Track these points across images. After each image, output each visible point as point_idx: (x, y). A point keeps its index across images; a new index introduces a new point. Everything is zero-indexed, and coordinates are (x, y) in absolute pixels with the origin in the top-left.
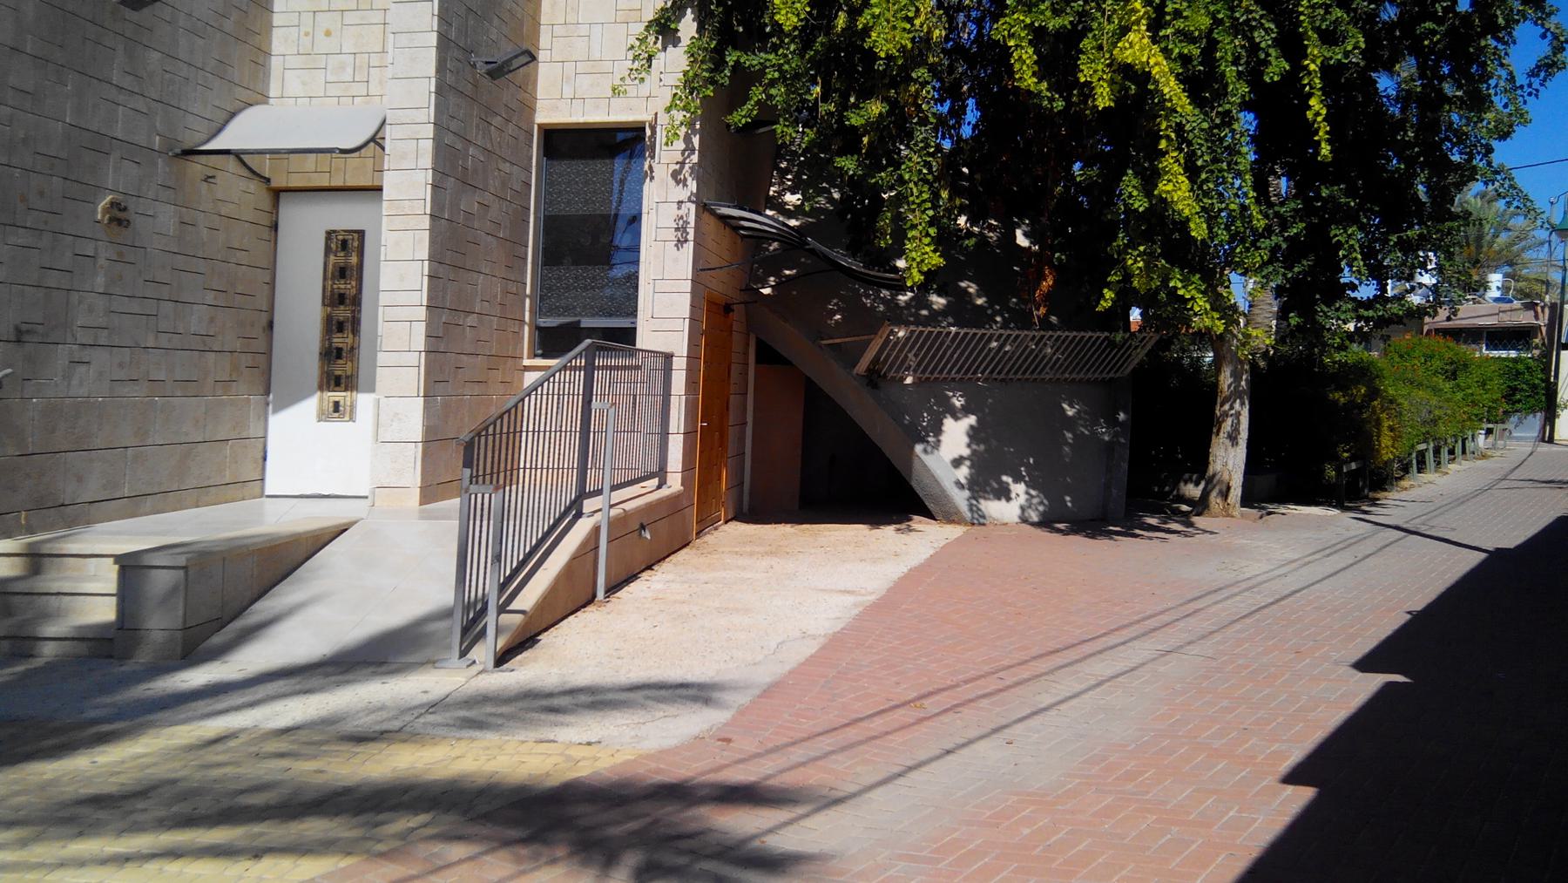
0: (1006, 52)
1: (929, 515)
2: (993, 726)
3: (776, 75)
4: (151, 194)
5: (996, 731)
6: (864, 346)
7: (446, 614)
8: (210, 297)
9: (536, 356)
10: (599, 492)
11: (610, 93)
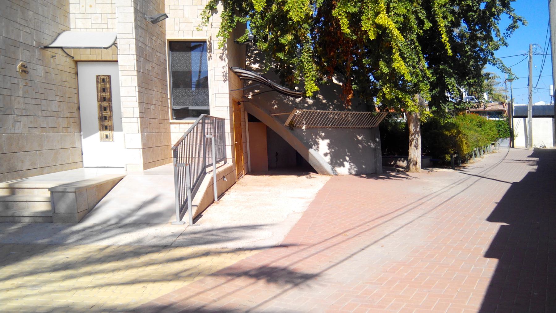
0: (338, 21)
1: (315, 172)
3: (254, 25)
4: (34, 62)
5: (375, 242)
6: (287, 117)
8: (58, 98)
10: (212, 165)
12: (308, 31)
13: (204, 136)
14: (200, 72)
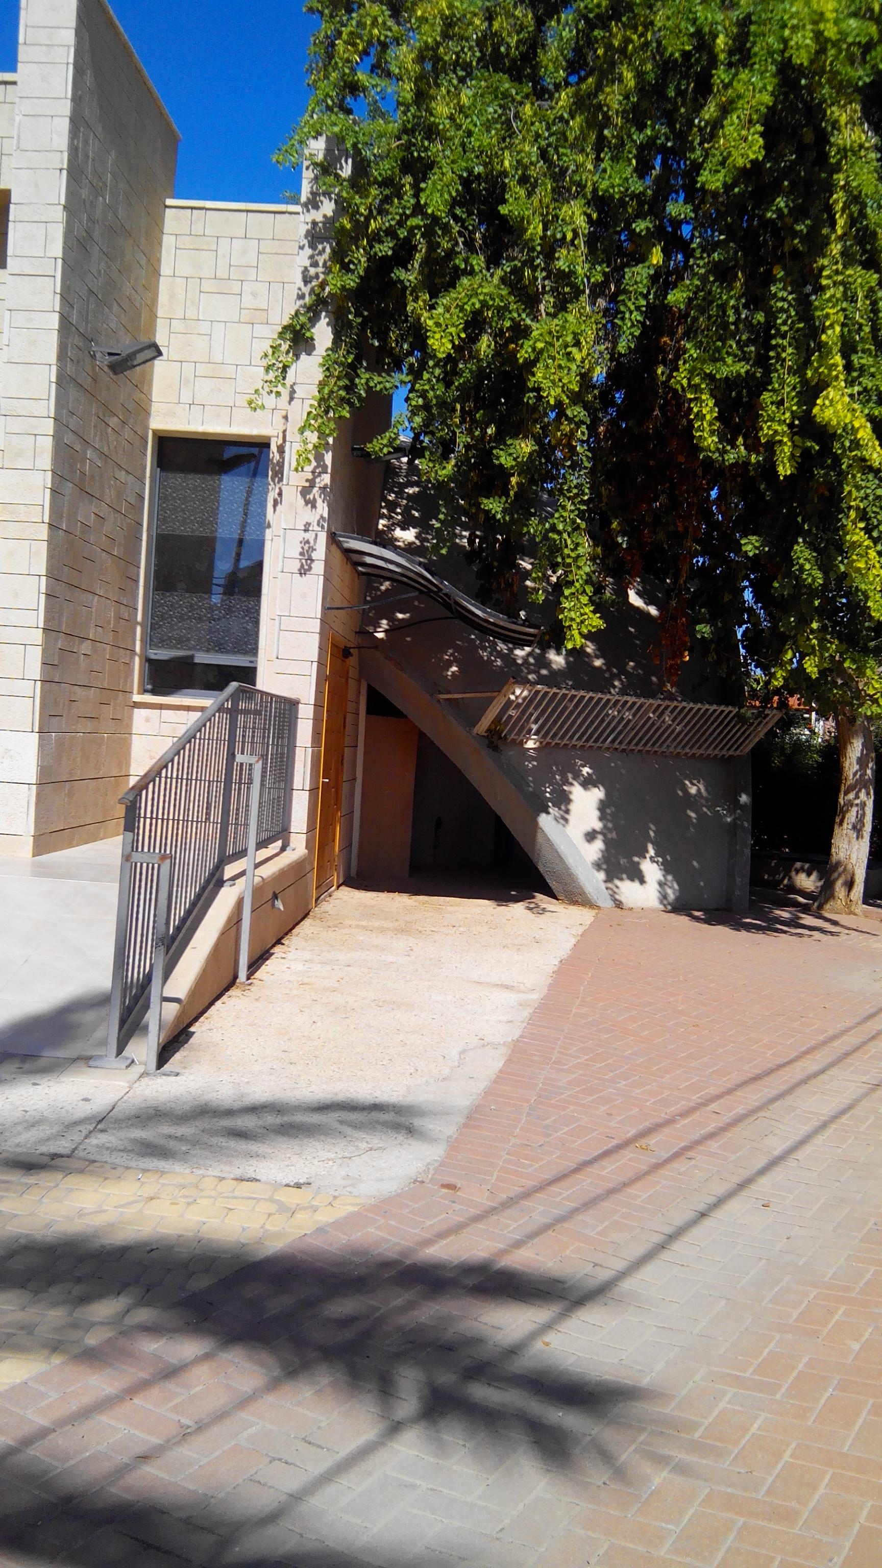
1: (551, 894)
2: (736, 1180)
3: (421, 401)
7: (100, 1001)
9: (145, 691)
10: (241, 854)
11: (242, 401)
12: (584, 428)
13: (231, 756)
14: (241, 542)
